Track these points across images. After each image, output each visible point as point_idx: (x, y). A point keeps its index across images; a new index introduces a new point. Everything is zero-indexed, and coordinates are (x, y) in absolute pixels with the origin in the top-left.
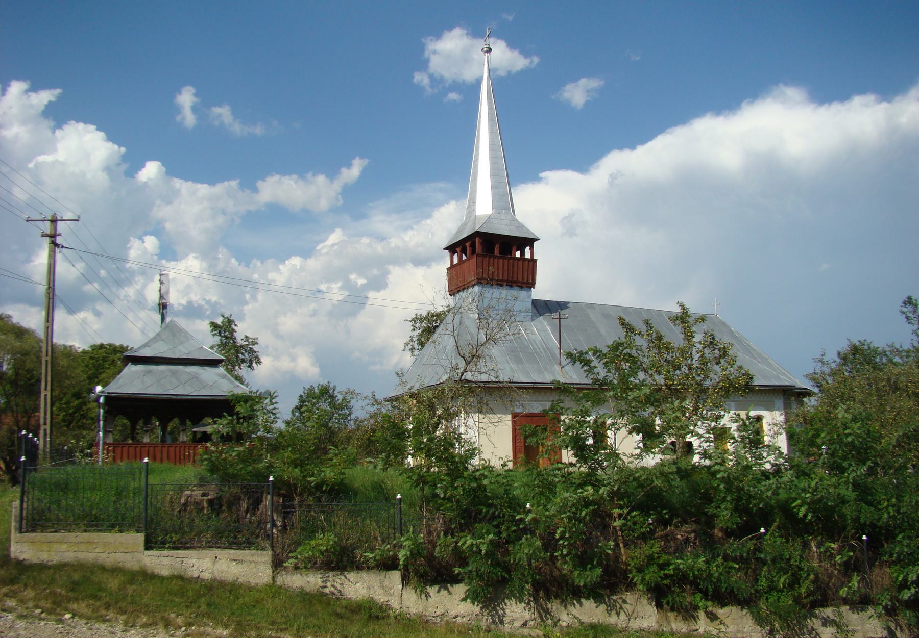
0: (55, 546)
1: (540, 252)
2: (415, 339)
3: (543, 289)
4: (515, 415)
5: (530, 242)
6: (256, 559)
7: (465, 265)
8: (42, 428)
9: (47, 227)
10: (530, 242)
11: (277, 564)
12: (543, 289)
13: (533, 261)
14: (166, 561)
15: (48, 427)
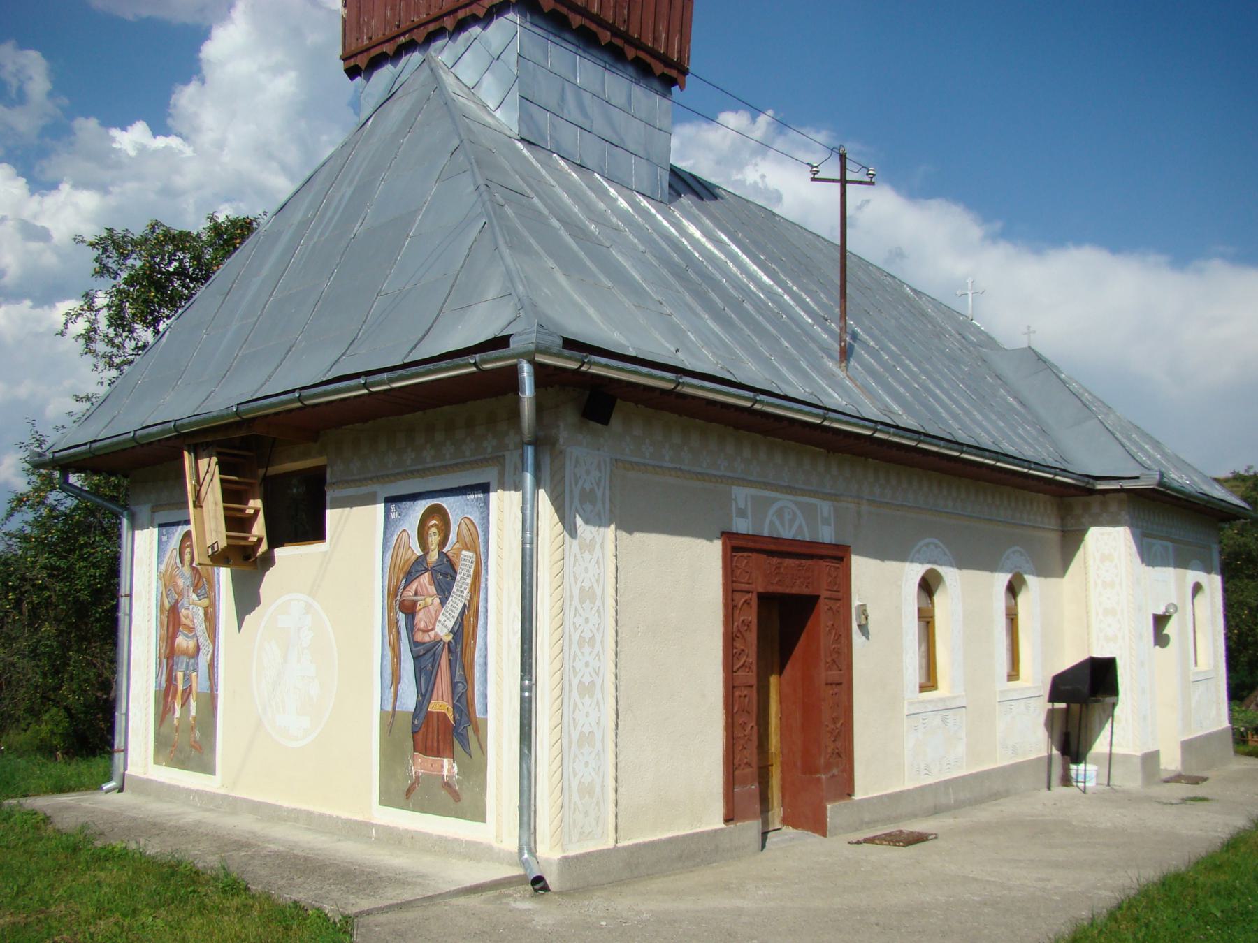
4: (738, 548)
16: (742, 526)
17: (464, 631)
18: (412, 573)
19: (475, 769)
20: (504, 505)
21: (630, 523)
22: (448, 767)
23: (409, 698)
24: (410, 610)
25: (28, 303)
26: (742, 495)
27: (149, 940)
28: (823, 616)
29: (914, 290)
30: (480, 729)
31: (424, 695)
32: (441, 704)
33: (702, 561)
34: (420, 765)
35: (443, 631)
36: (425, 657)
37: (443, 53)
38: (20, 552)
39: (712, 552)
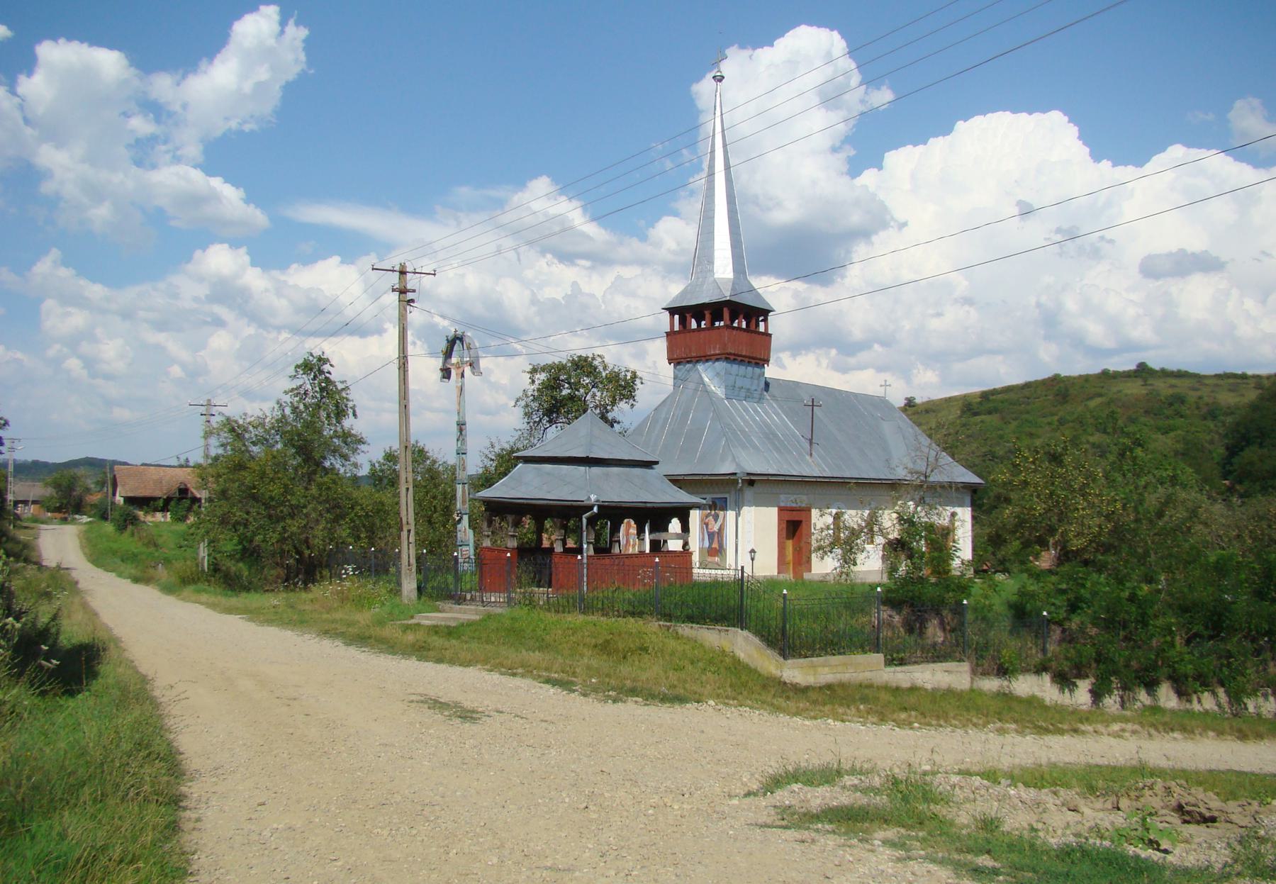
0: (820, 669)
6: (960, 669)
7: (702, 334)
8: (405, 529)
9: (394, 279)
10: (764, 313)
11: (973, 672)
13: (767, 335)
14: (900, 676)
15: (412, 528)
16: (782, 504)
17: (721, 529)
19: (724, 558)
20: (886, 512)
21: (757, 505)
23: (707, 544)
24: (707, 525)
25: (879, 657)
27: (3, 846)
28: (804, 524)
29: (1083, 733)
30: (725, 551)
31: (711, 543)
32: (715, 545)
33: (772, 513)
34: (710, 559)
35: (716, 528)
36: (711, 535)
37: (700, 367)
38: (1040, 508)
39: (776, 509)
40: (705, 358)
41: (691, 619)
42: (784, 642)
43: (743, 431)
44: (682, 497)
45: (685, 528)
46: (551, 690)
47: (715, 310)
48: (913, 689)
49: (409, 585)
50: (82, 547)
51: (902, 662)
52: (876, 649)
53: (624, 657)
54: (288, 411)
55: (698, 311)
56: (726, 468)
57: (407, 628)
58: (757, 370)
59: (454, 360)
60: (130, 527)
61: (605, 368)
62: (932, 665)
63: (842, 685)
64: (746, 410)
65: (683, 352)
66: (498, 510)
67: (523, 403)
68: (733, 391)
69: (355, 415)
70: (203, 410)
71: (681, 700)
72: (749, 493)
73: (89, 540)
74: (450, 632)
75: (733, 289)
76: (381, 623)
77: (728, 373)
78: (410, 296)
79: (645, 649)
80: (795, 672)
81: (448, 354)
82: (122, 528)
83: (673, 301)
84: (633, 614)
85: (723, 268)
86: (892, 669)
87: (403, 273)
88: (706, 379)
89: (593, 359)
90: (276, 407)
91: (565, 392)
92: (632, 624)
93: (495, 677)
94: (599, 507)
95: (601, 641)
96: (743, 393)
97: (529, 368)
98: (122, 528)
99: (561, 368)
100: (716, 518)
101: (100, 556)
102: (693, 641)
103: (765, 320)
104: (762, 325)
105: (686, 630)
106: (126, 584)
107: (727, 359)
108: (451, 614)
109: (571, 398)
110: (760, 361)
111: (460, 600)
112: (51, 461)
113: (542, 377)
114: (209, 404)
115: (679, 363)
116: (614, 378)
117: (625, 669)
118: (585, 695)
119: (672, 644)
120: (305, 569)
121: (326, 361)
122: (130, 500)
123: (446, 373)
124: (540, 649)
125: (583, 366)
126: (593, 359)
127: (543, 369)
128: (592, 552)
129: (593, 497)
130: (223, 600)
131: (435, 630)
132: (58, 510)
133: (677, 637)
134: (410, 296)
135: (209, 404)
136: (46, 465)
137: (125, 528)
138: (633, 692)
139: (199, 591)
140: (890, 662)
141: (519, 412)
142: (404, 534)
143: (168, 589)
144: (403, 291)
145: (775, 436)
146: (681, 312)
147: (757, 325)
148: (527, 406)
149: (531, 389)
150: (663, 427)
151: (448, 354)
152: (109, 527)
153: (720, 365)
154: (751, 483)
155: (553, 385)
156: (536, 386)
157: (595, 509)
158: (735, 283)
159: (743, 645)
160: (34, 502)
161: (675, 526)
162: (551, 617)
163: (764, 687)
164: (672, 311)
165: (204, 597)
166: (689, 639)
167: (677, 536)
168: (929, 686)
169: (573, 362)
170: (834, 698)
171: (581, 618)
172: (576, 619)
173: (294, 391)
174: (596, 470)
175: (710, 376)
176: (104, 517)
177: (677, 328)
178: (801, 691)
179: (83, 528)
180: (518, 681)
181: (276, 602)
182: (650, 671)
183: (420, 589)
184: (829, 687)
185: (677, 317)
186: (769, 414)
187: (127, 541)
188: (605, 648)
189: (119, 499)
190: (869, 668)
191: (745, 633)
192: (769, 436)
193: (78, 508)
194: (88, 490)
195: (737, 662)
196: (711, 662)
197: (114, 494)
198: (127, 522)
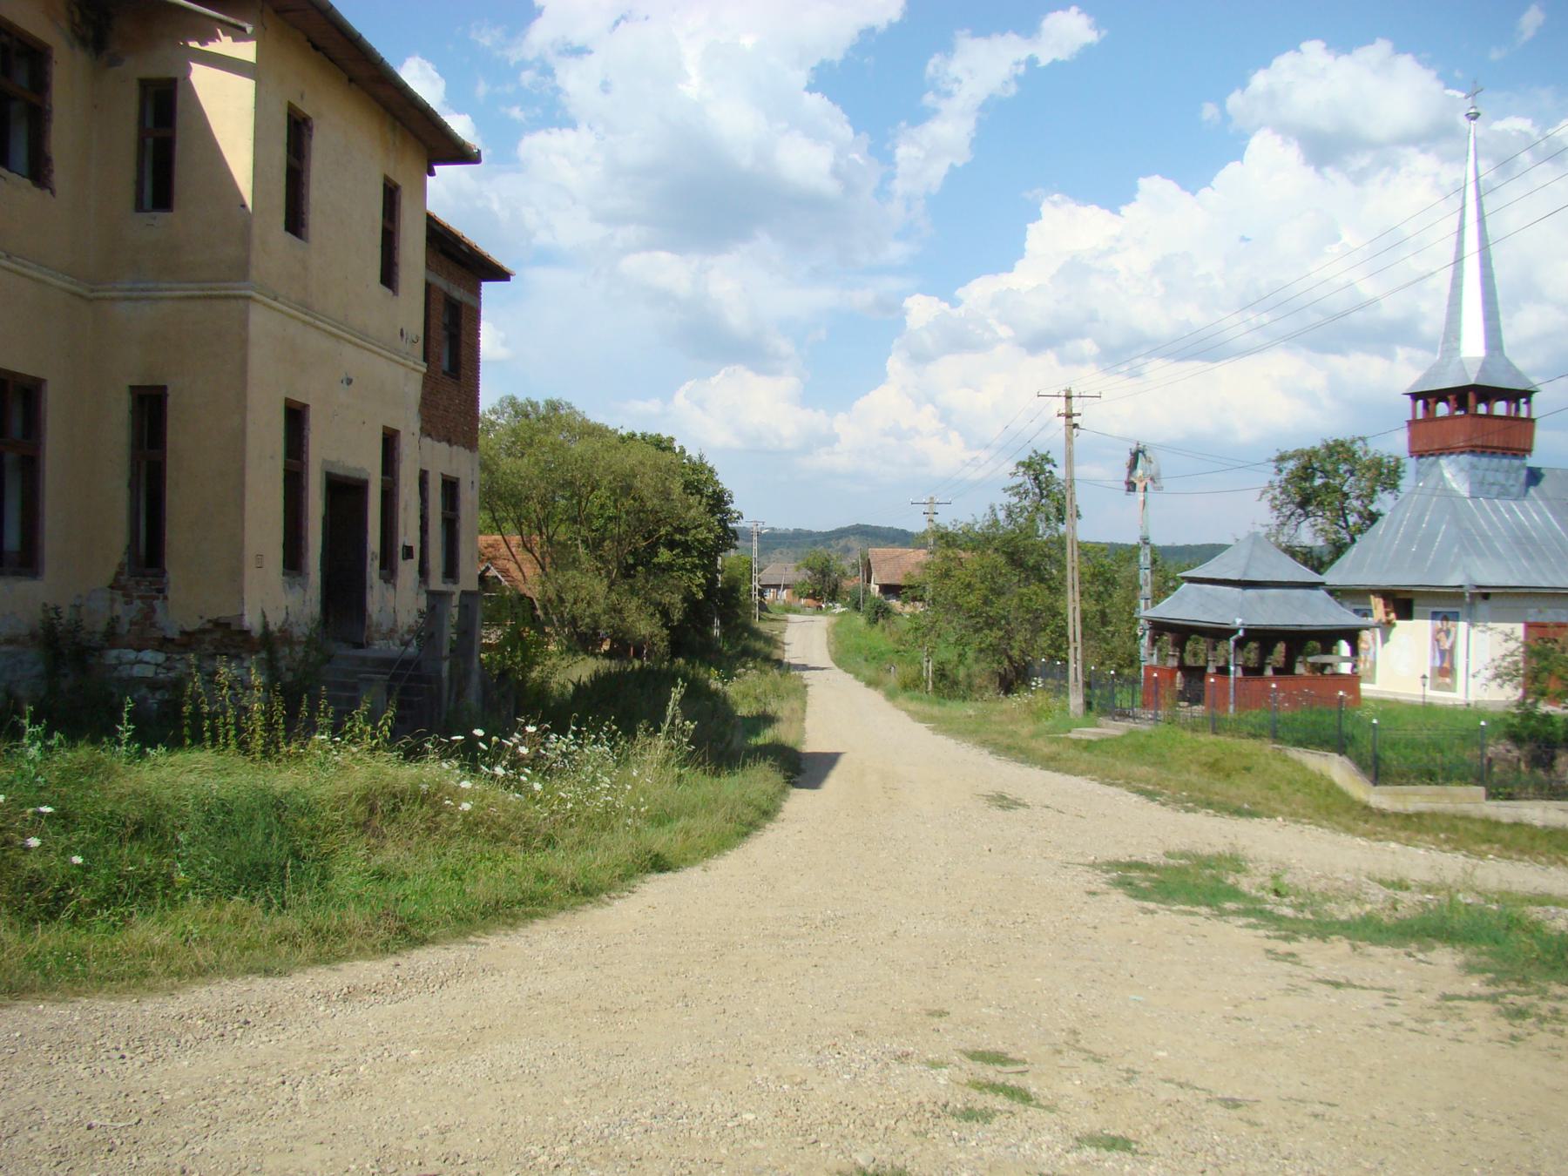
1: (1539, 407)
2: (1276, 484)
3: (1531, 462)
4: (1529, 626)
5: (1527, 394)
10: (1527, 394)
12: (1531, 462)
13: (1530, 421)
14: (1507, 810)
15: (1079, 645)
16: (1530, 620)
17: (1452, 647)
18: (1440, 631)
19: (1454, 681)
22: (1448, 680)
23: (1438, 663)
25: (1481, 790)
26: (1532, 611)
32: (1446, 665)
34: (1440, 680)
36: (1442, 653)
37: (1443, 461)
39: (1519, 629)
40: (1446, 451)
41: (1299, 743)
42: (1377, 772)
43: (1485, 538)
44: (1343, 617)
45: (1355, 651)
46: (1134, 798)
47: (1460, 396)
48: (1517, 825)
49: (1076, 700)
50: (829, 643)
51: (1510, 797)
52: (1479, 781)
53: (1228, 776)
54: (1001, 515)
55: (1441, 395)
56: (1454, 579)
57: (1053, 741)
58: (1516, 462)
59: (1139, 472)
60: (881, 621)
61: (1366, 453)
62: (1545, 803)
63: (1434, 815)
64: (1496, 510)
65: (1429, 441)
66: (1159, 628)
67: (1269, 496)
68: (1480, 488)
69: (1078, 516)
70: (925, 508)
71: (1251, 814)
72: (1482, 607)
73: (836, 634)
74: (1089, 746)
75: (1483, 370)
76: (1034, 736)
77: (1473, 467)
78: (1075, 420)
79: (1248, 769)
80: (1381, 798)
81: (1133, 466)
82: (873, 621)
83: (1427, 376)
84: (1254, 736)
85: (1473, 346)
86: (1494, 803)
87: (1068, 397)
88: (1447, 475)
89: (1353, 442)
90: (989, 511)
91: (1318, 482)
92: (1248, 745)
93: (1095, 785)
94: (1246, 631)
95: (1211, 760)
96: (1495, 489)
97: (1275, 455)
98: (873, 621)
99: (1313, 453)
100: (1447, 632)
101: (845, 656)
102: (1299, 763)
103: (1528, 402)
104: (1523, 408)
105: (1295, 753)
106: (859, 686)
107: (1472, 452)
108: (1112, 728)
109: (1326, 485)
110: (1526, 451)
111: (1124, 715)
112: (815, 530)
113: (1291, 465)
114: (932, 502)
115: (1421, 456)
116: (1377, 464)
117: (1219, 786)
118: (1163, 805)
119: (1277, 765)
120: (1012, 680)
121: (1049, 461)
122: (888, 589)
123: (1131, 486)
124: (1153, 764)
125: (1339, 451)
126: (1353, 442)
127: (1291, 457)
128: (1240, 674)
129: (1239, 621)
130: (936, 710)
131: (1076, 743)
132: (813, 596)
133: (1286, 760)
134: (1075, 420)
135: (932, 502)
136: (810, 534)
137: (876, 621)
138: (1209, 805)
139: (912, 699)
140: (1492, 796)
141: (1265, 504)
142: (1071, 651)
143: (891, 696)
144: (1069, 416)
145: (1529, 538)
146: (1427, 398)
147: (1518, 409)
148: (1275, 498)
149: (1277, 479)
150: (1397, 531)
151: (1133, 466)
152: (860, 620)
153: (1465, 459)
154: (1486, 596)
155: (1306, 472)
156: (1284, 475)
157: (1241, 633)
158: (1485, 366)
159: (1337, 769)
160: (786, 587)
161: (1344, 648)
162: (1188, 735)
163: (1348, 810)
164: (1415, 396)
165: (913, 706)
166: (1292, 760)
167: (1345, 660)
168: (1538, 823)
169: (1328, 447)
170: (1412, 825)
171: (1213, 738)
172: (1206, 738)
173: (1017, 491)
174: (1250, 593)
175: (1453, 473)
176: (857, 608)
177: (1420, 416)
178: (1383, 814)
179: (834, 620)
180: (1112, 790)
181: (971, 712)
182: (1245, 789)
183: (1088, 705)
184: (1419, 815)
185: (1420, 403)
186: (1532, 513)
187: (879, 638)
188: (1214, 766)
189: (875, 588)
190: (1469, 800)
191: (1344, 759)
192: (1524, 542)
193: (834, 595)
194: (844, 574)
195: (1332, 784)
196: (1306, 784)
197: (869, 581)
198: (880, 613)
